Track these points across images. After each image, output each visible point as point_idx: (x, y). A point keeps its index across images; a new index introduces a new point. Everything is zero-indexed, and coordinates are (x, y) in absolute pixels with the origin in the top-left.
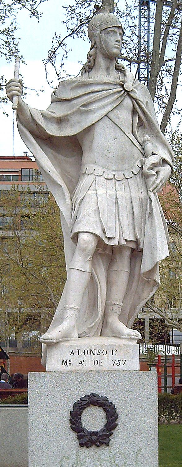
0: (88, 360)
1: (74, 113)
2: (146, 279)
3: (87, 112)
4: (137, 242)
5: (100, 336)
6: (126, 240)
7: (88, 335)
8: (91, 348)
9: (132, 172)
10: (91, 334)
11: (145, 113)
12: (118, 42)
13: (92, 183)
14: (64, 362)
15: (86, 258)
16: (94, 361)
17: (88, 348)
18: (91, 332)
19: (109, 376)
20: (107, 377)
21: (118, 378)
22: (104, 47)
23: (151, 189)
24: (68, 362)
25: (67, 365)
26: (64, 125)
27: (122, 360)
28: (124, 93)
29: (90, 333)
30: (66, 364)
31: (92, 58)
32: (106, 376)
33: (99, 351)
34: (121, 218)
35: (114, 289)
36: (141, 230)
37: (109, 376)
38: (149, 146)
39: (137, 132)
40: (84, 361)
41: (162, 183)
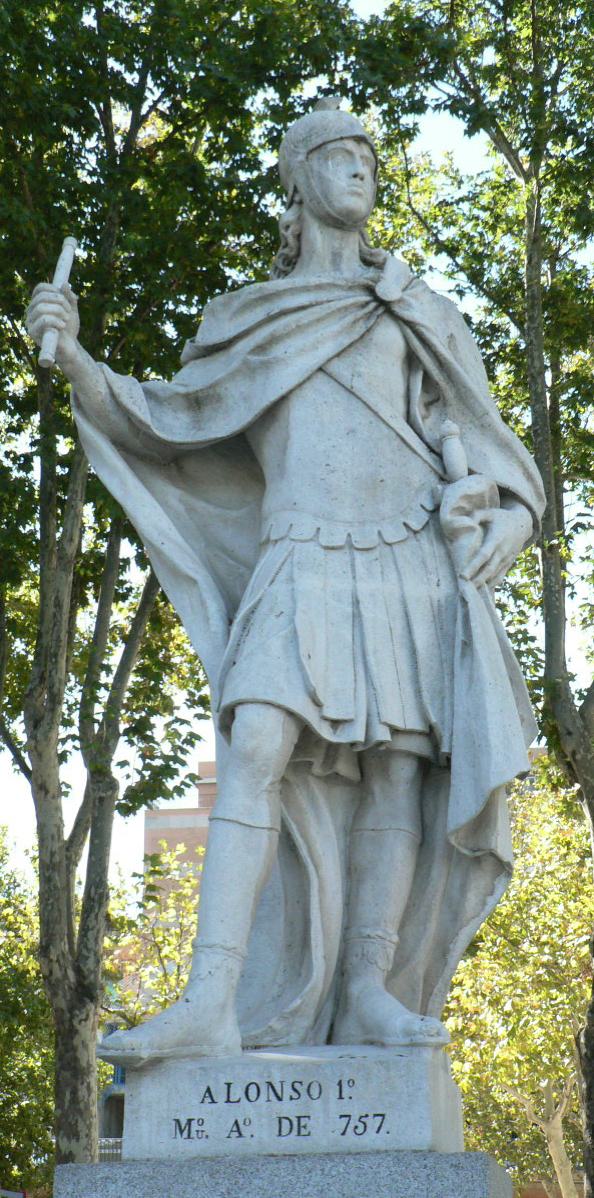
0: (261, 1117)
1: (232, 376)
2: (466, 852)
3: (266, 365)
4: (431, 734)
5: (329, 1041)
6: (395, 731)
7: (283, 1041)
8: (269, 1077)
9: (405, 524)
10: (292, 1035)
11: (443, 361)
12: (358, 179)
13: (283, 564)
14: (180, 1127)
15: (260, 782)
16: (280, 1122)
17: (261, 1076)
18: (294, 1028)
19: (323, 1170)
20: (316, 1175)
21: (353, 1178)
22: (318, 194)
23: (467, 573)
24: (195, 1126)
25: (189, 1137)
26: (207, 411)
27: (371, 1115)
28: (376, 309)
29: (288, 1034)
30: (185, 1133)
31: (290, 231)
32: (314, 1173)
33: (297, 1086)
34: (371, 659)
35: (367, 893)
36: (443, 699)
37: (323, 1170)
38: (457, 454)
39: (424, 418)
40: (248, 1122)
41: (503, 556)
